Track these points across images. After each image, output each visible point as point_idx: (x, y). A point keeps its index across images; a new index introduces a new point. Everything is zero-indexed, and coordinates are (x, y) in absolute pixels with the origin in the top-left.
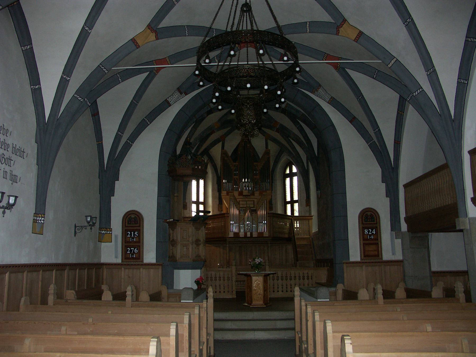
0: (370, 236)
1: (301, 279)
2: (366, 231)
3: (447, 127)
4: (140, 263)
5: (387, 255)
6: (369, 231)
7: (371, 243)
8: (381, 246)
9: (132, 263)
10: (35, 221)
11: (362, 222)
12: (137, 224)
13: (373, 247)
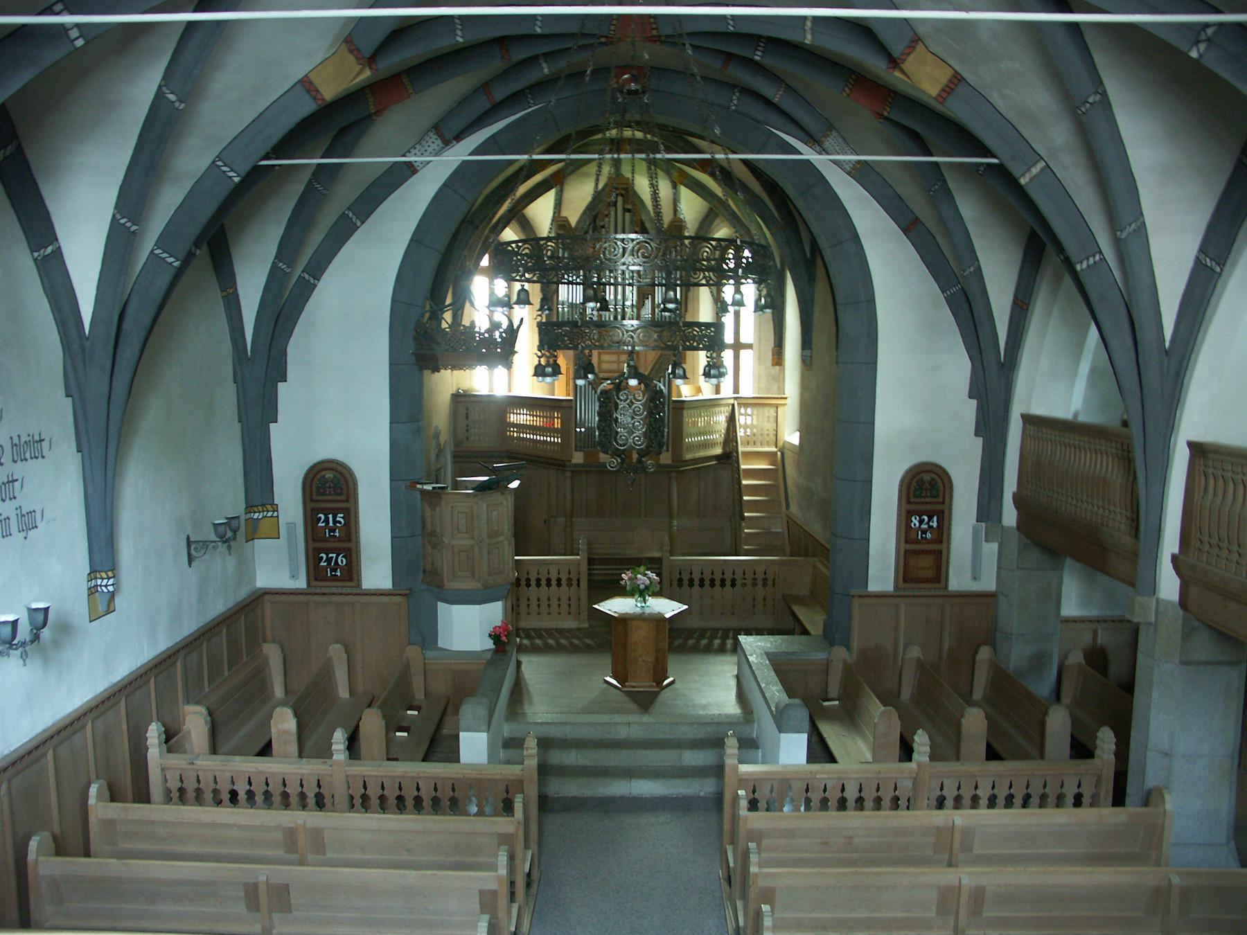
0: (924, 532)
1: (749, 586)
2: (915, 521)
3: (1150, 369)
4: (354, 591)
5: (959, 579)
6: (921, 522)
7: (924, 554)
8: (948, 558)
9: (334, 590)
10: (92, 591)
11: (908, 497)
12: (340, 494)
13: (926, 562)
